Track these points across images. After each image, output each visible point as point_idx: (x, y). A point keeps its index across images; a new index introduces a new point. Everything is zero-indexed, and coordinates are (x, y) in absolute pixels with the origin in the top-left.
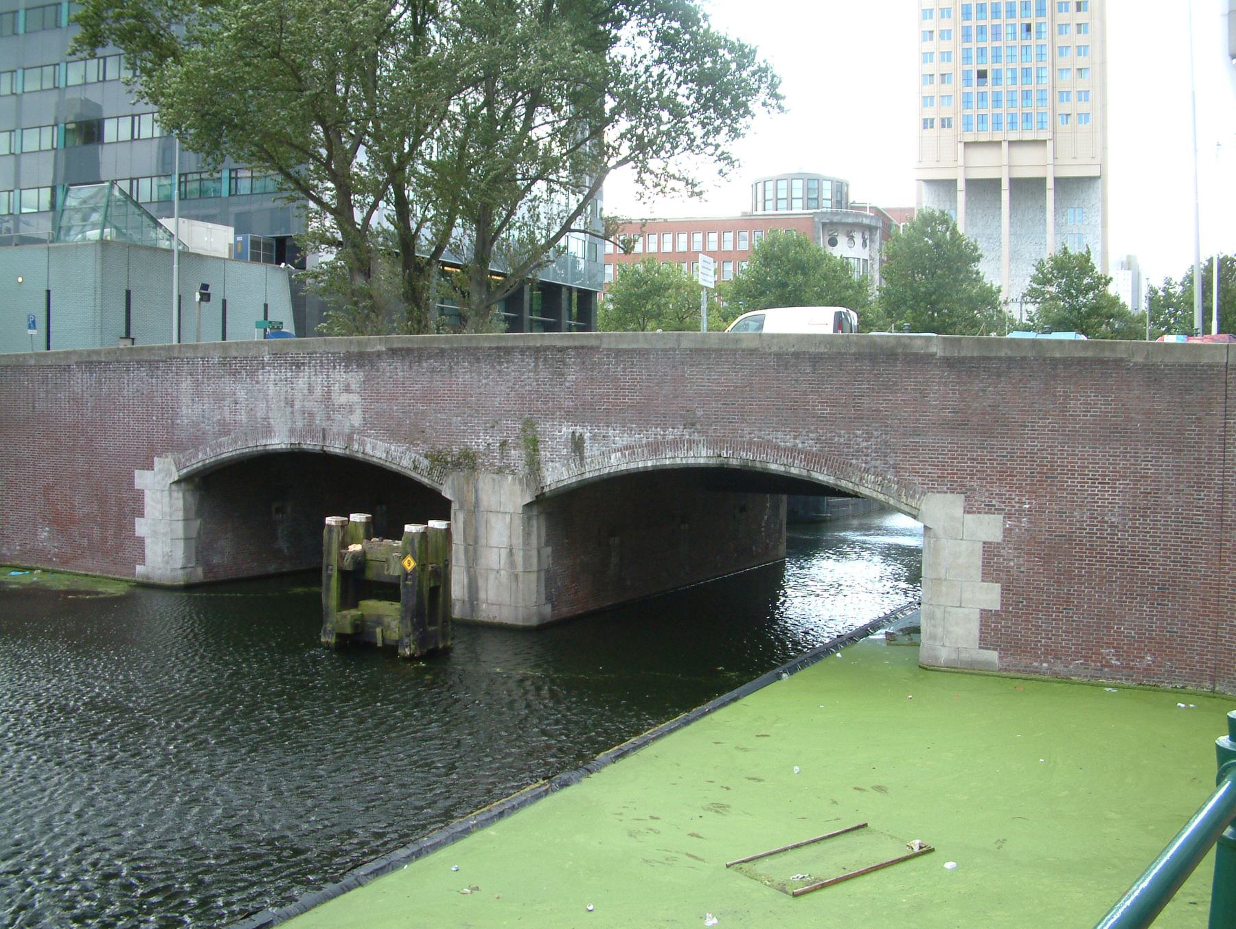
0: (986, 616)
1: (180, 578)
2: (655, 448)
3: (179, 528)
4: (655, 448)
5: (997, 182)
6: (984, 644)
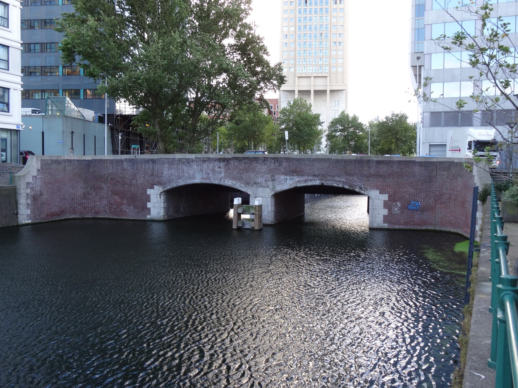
0: (385, 216)
1: (162, 218)
2: (306, 181)
3: (162, 205)
4: (306, 181)
5: (294, 91)
6: (384, 222)
